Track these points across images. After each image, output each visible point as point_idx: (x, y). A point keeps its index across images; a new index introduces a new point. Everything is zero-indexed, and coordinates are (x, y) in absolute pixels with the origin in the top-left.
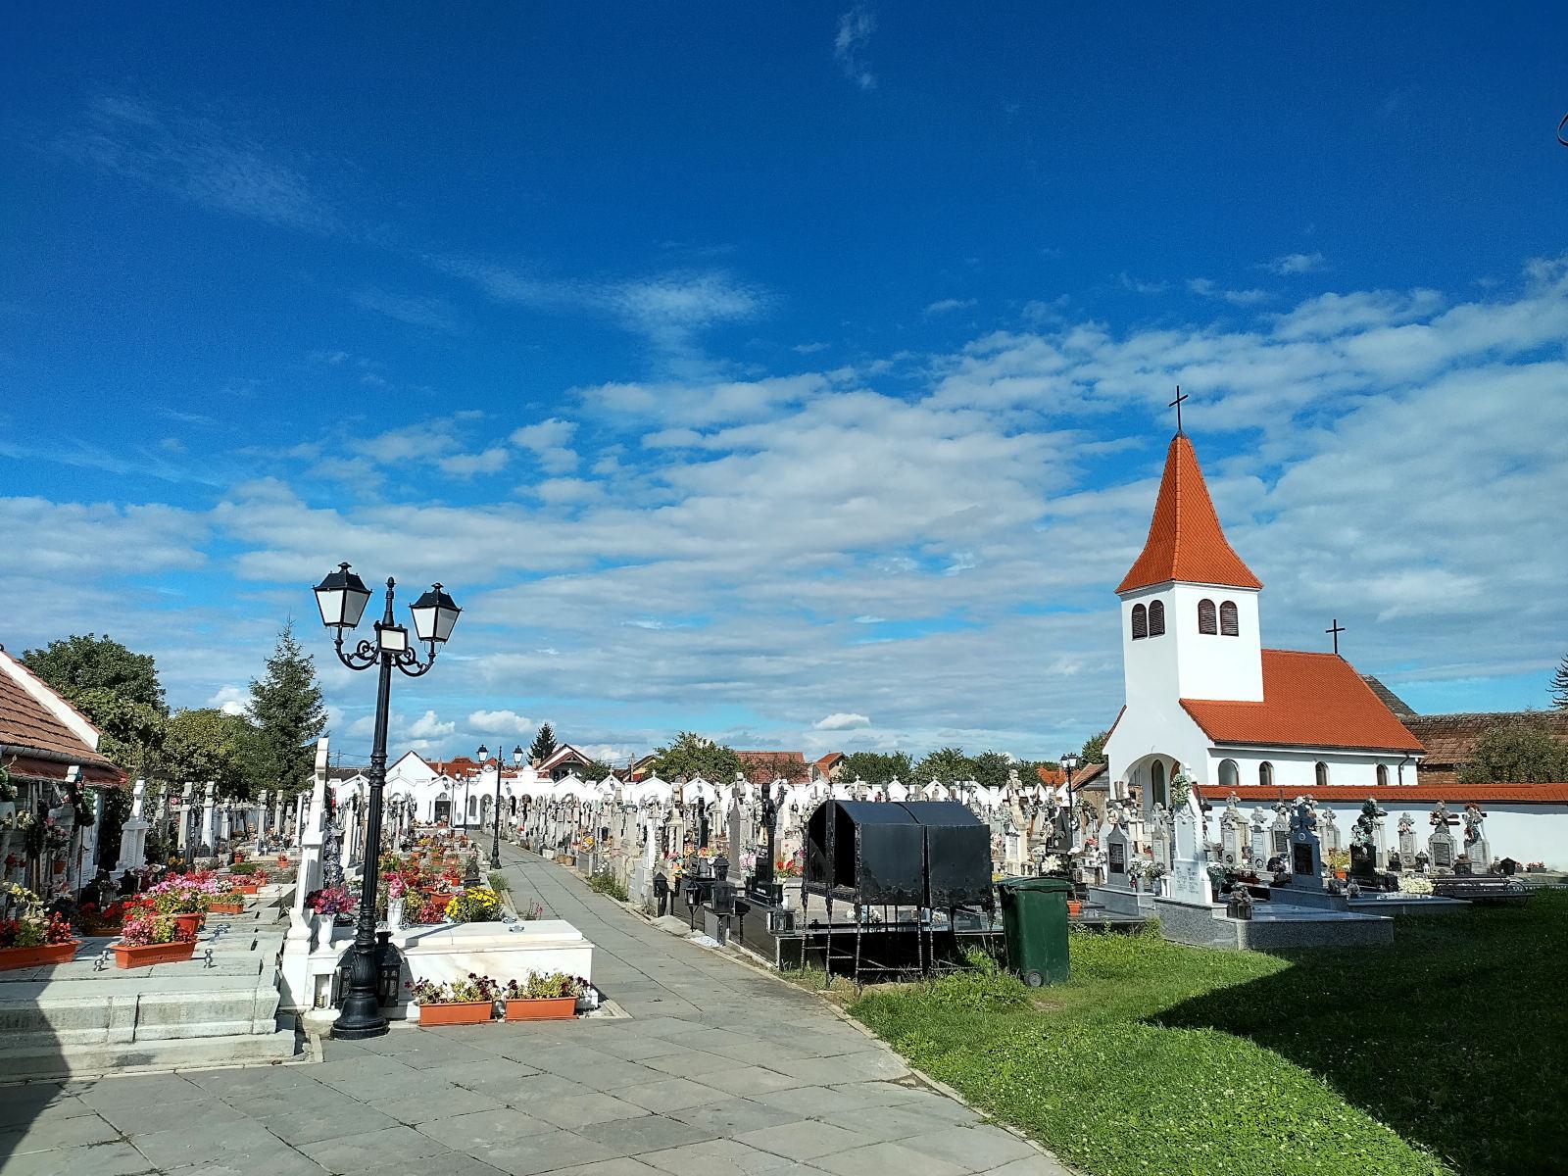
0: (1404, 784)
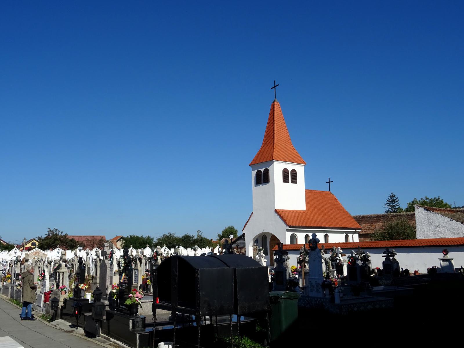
0: (354, 242)
